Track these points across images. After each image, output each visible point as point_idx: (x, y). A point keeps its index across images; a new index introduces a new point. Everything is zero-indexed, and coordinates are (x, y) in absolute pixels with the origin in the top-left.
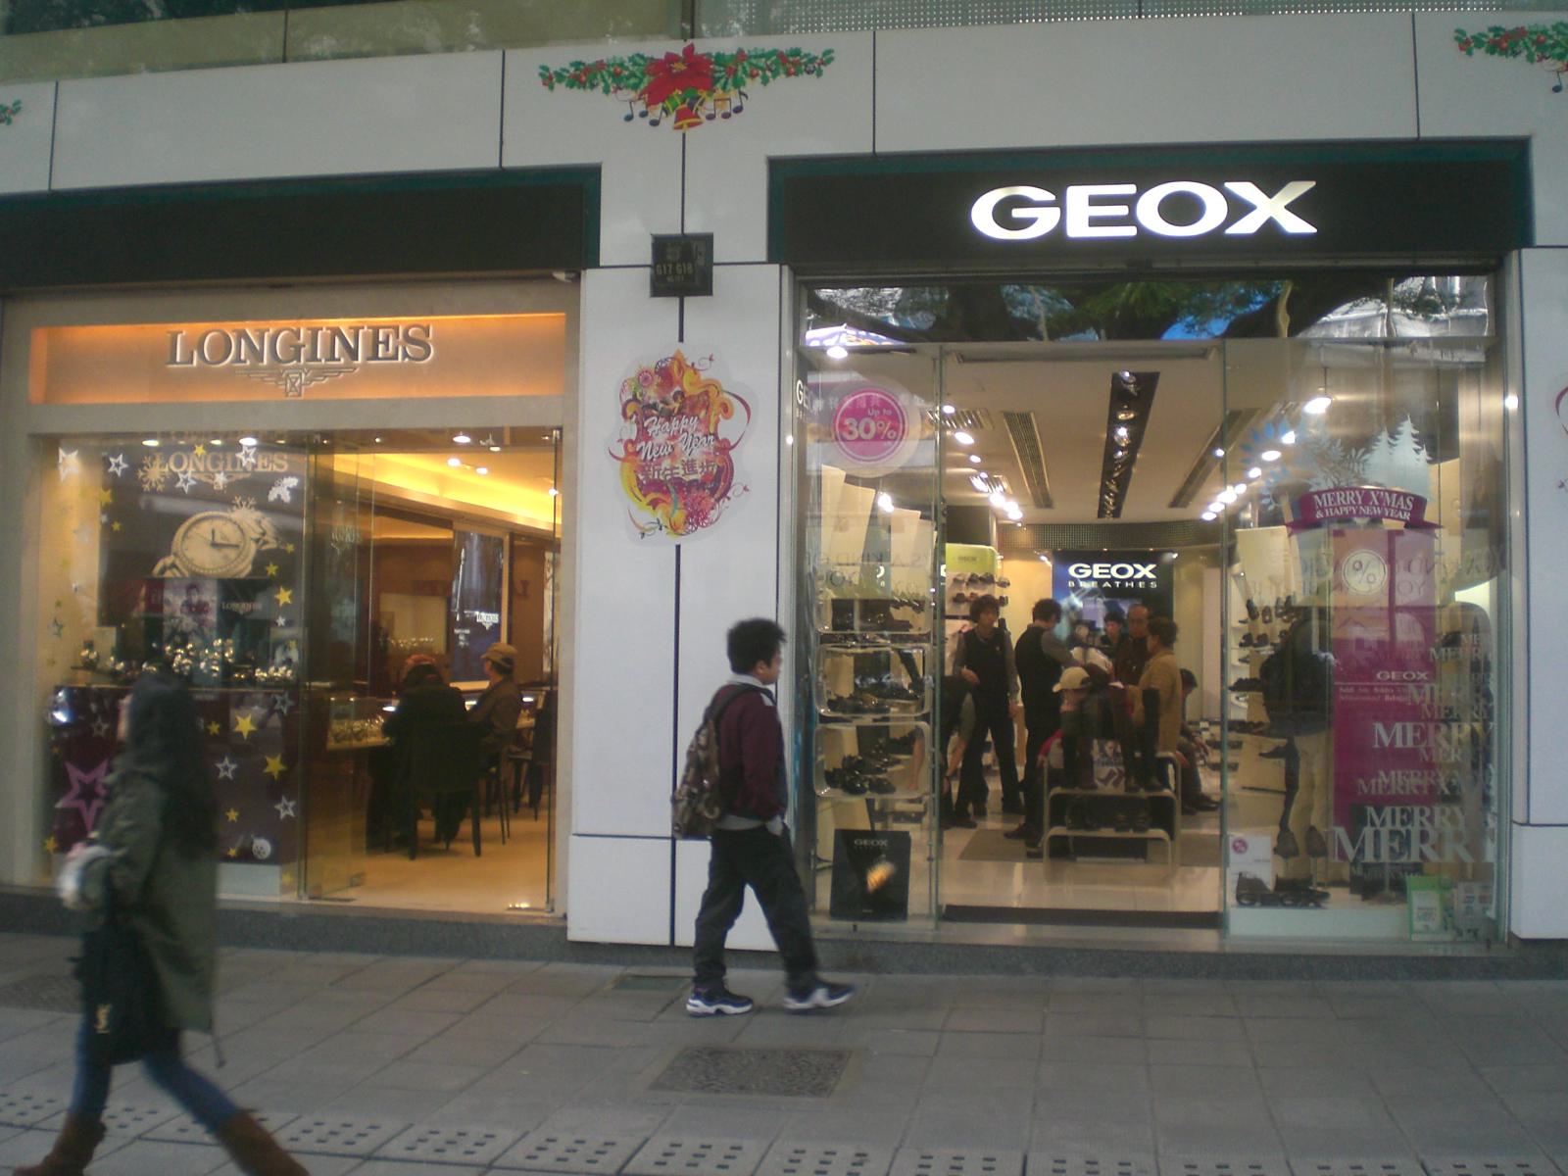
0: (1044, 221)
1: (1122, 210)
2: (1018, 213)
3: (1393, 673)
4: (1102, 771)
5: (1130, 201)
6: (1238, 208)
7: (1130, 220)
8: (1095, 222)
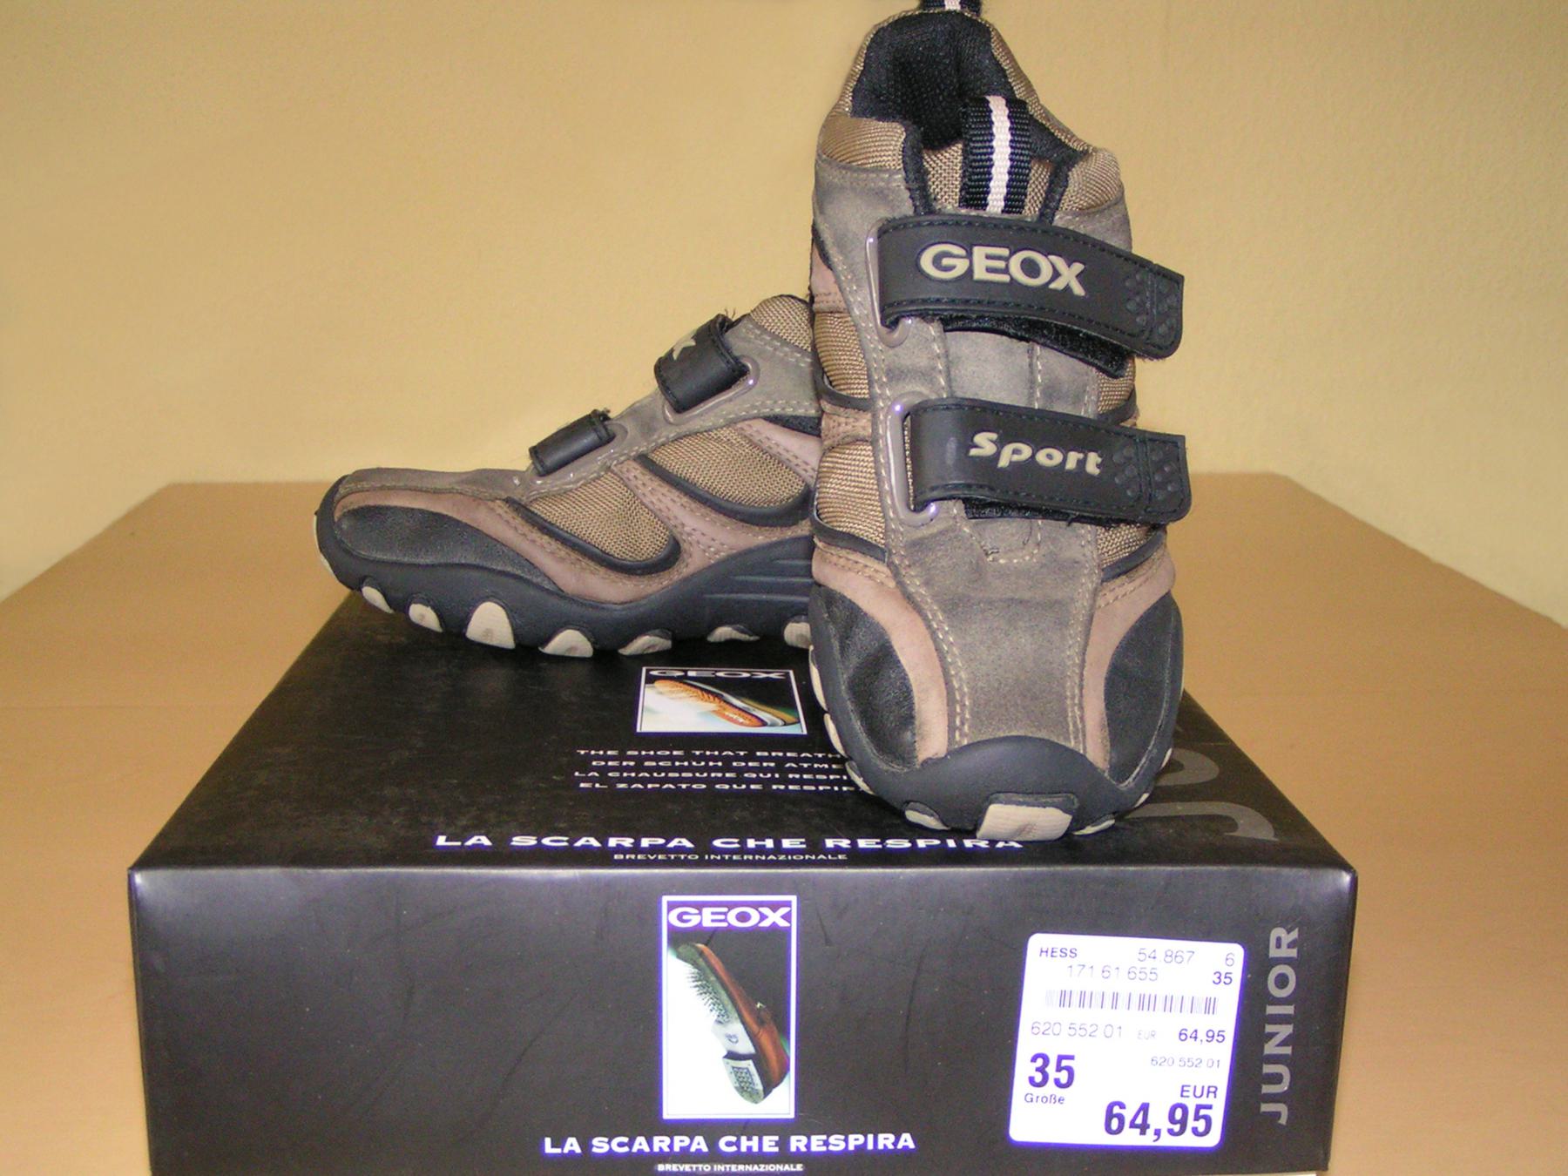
0: (694, 921)
1: (1001, 264)
2: (946, 262)
3: (979, 252)
4: (775, 918)
5: (1007, 259)
6: (763, 917)
7: (1006, 271)
8: (989, 270)
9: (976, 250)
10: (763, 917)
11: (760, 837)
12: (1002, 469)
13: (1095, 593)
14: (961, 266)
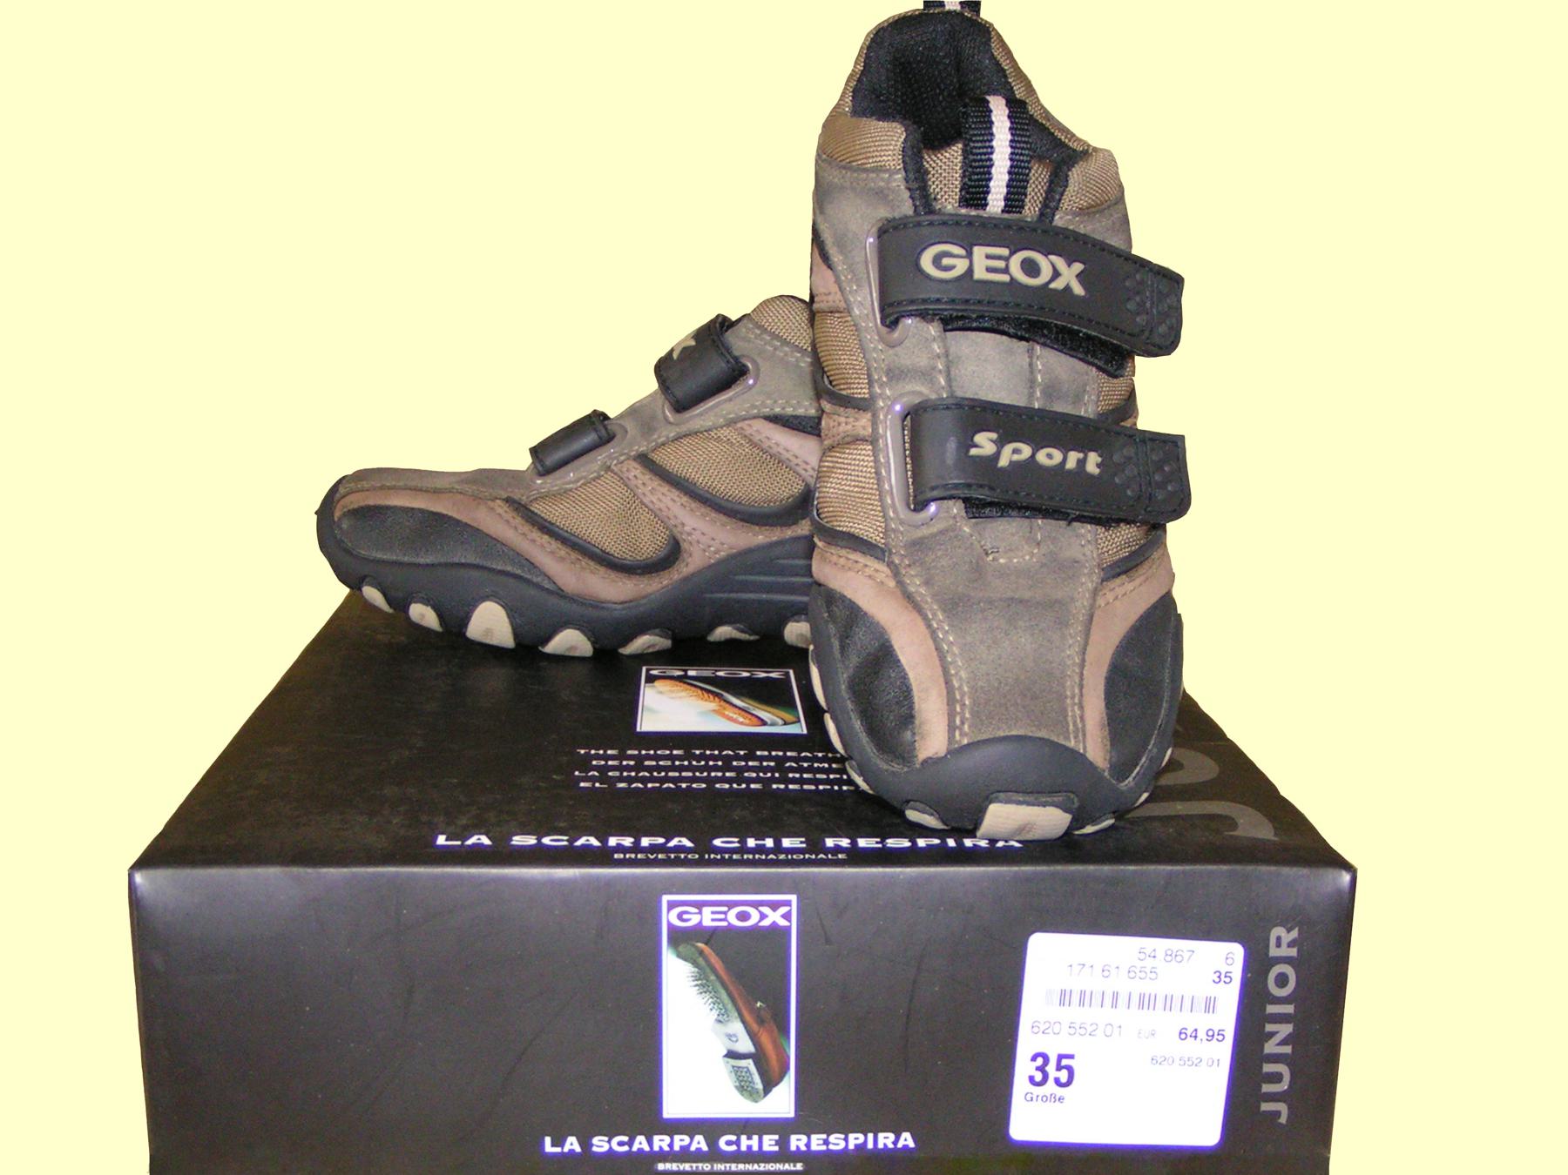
0: (694, 920)
1: (1002, 264)
2: (946, 261)
3: (979, 252)
4: (775, 917)
5: (1007, 259)
6: (763, 916)
7: (1006, 271)
8: (989, 270)
9: (976, 249)
10: (763, 916)
11: (760, 836)
12: (1002, 469)
14: (961, 266)
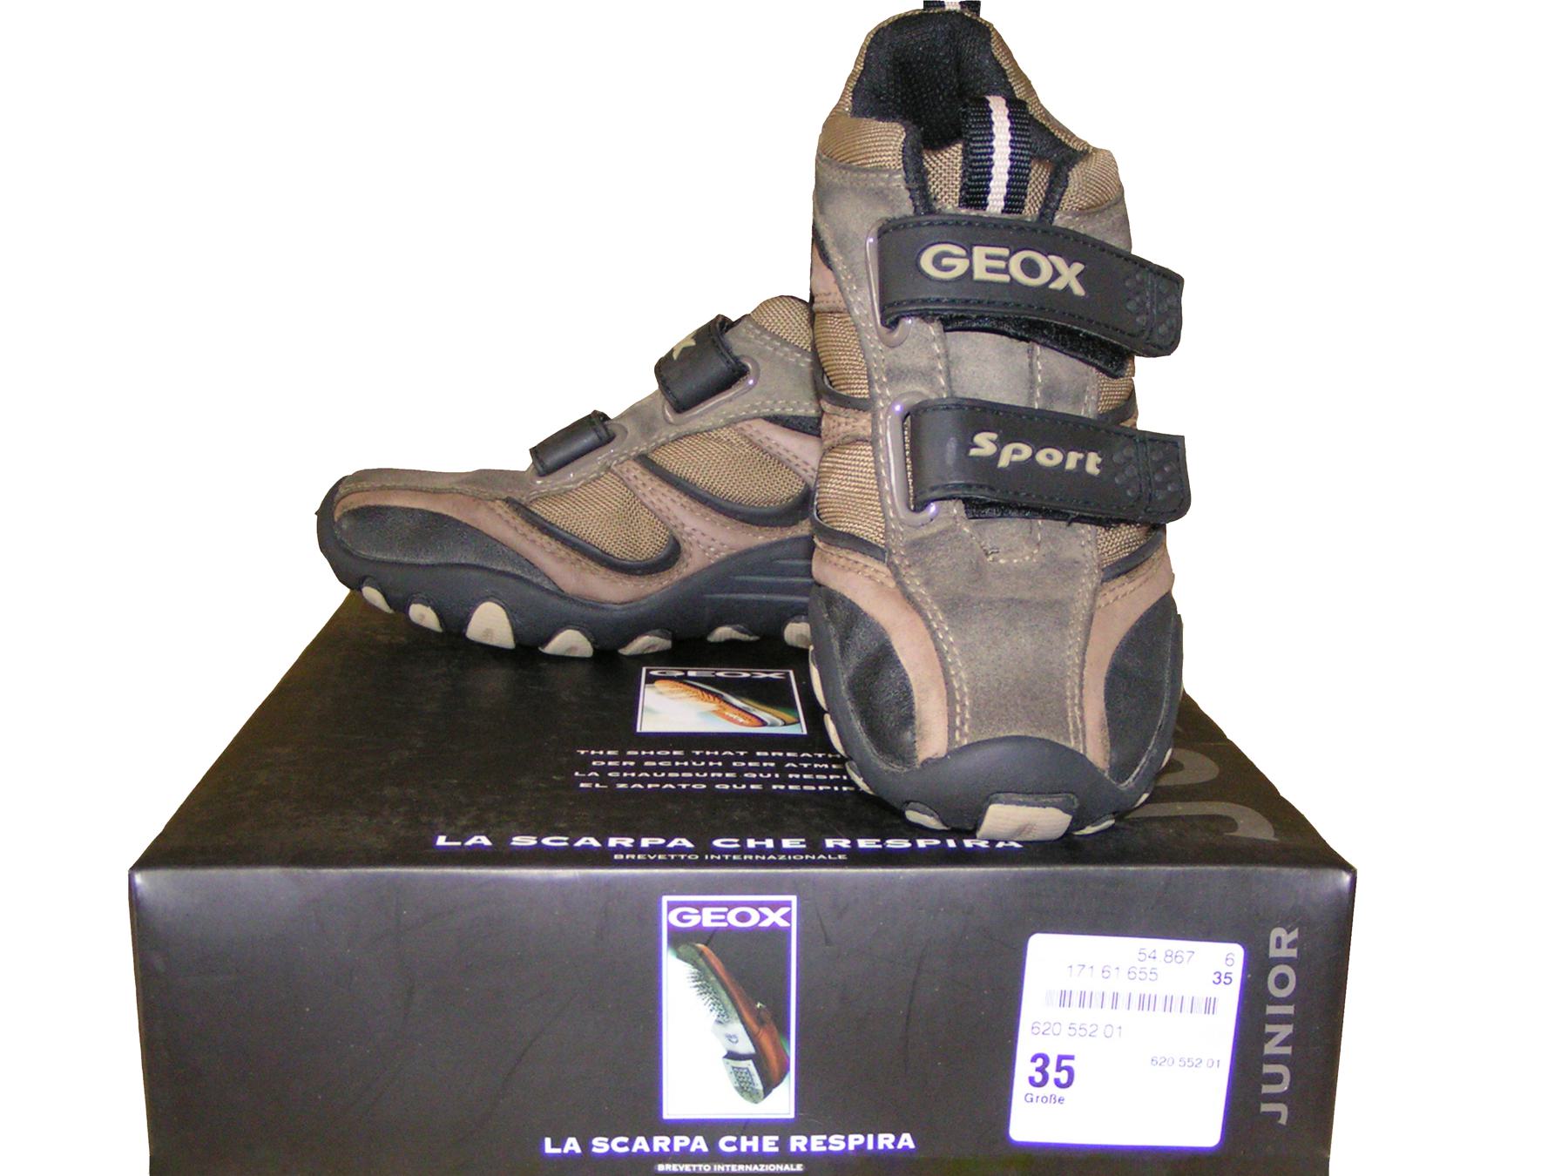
0: (694, 921)
1: (1002, 264)
2: (946, 262)
3: (979, 252)
5: (1007, 259)
6: (763, 917)
7: (1006, 271)
8: (989, 270)
9: (976, 250)
13: (1095, 593)
14: (961, 266)
